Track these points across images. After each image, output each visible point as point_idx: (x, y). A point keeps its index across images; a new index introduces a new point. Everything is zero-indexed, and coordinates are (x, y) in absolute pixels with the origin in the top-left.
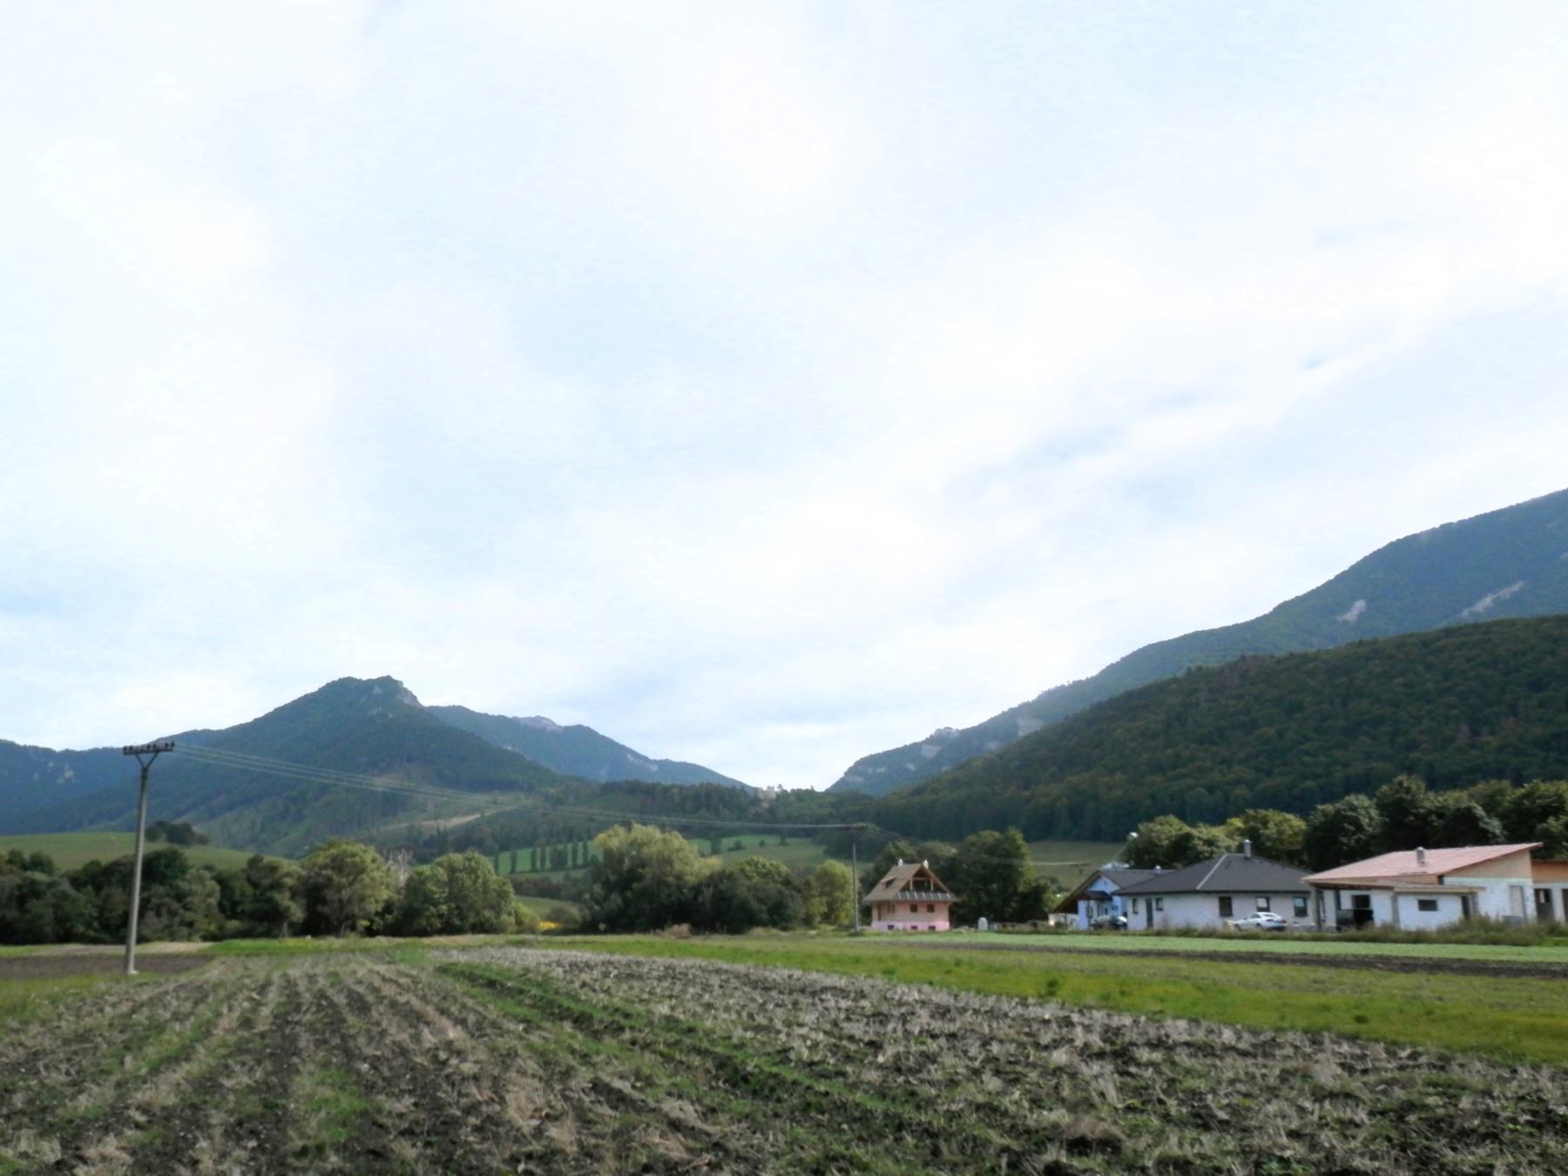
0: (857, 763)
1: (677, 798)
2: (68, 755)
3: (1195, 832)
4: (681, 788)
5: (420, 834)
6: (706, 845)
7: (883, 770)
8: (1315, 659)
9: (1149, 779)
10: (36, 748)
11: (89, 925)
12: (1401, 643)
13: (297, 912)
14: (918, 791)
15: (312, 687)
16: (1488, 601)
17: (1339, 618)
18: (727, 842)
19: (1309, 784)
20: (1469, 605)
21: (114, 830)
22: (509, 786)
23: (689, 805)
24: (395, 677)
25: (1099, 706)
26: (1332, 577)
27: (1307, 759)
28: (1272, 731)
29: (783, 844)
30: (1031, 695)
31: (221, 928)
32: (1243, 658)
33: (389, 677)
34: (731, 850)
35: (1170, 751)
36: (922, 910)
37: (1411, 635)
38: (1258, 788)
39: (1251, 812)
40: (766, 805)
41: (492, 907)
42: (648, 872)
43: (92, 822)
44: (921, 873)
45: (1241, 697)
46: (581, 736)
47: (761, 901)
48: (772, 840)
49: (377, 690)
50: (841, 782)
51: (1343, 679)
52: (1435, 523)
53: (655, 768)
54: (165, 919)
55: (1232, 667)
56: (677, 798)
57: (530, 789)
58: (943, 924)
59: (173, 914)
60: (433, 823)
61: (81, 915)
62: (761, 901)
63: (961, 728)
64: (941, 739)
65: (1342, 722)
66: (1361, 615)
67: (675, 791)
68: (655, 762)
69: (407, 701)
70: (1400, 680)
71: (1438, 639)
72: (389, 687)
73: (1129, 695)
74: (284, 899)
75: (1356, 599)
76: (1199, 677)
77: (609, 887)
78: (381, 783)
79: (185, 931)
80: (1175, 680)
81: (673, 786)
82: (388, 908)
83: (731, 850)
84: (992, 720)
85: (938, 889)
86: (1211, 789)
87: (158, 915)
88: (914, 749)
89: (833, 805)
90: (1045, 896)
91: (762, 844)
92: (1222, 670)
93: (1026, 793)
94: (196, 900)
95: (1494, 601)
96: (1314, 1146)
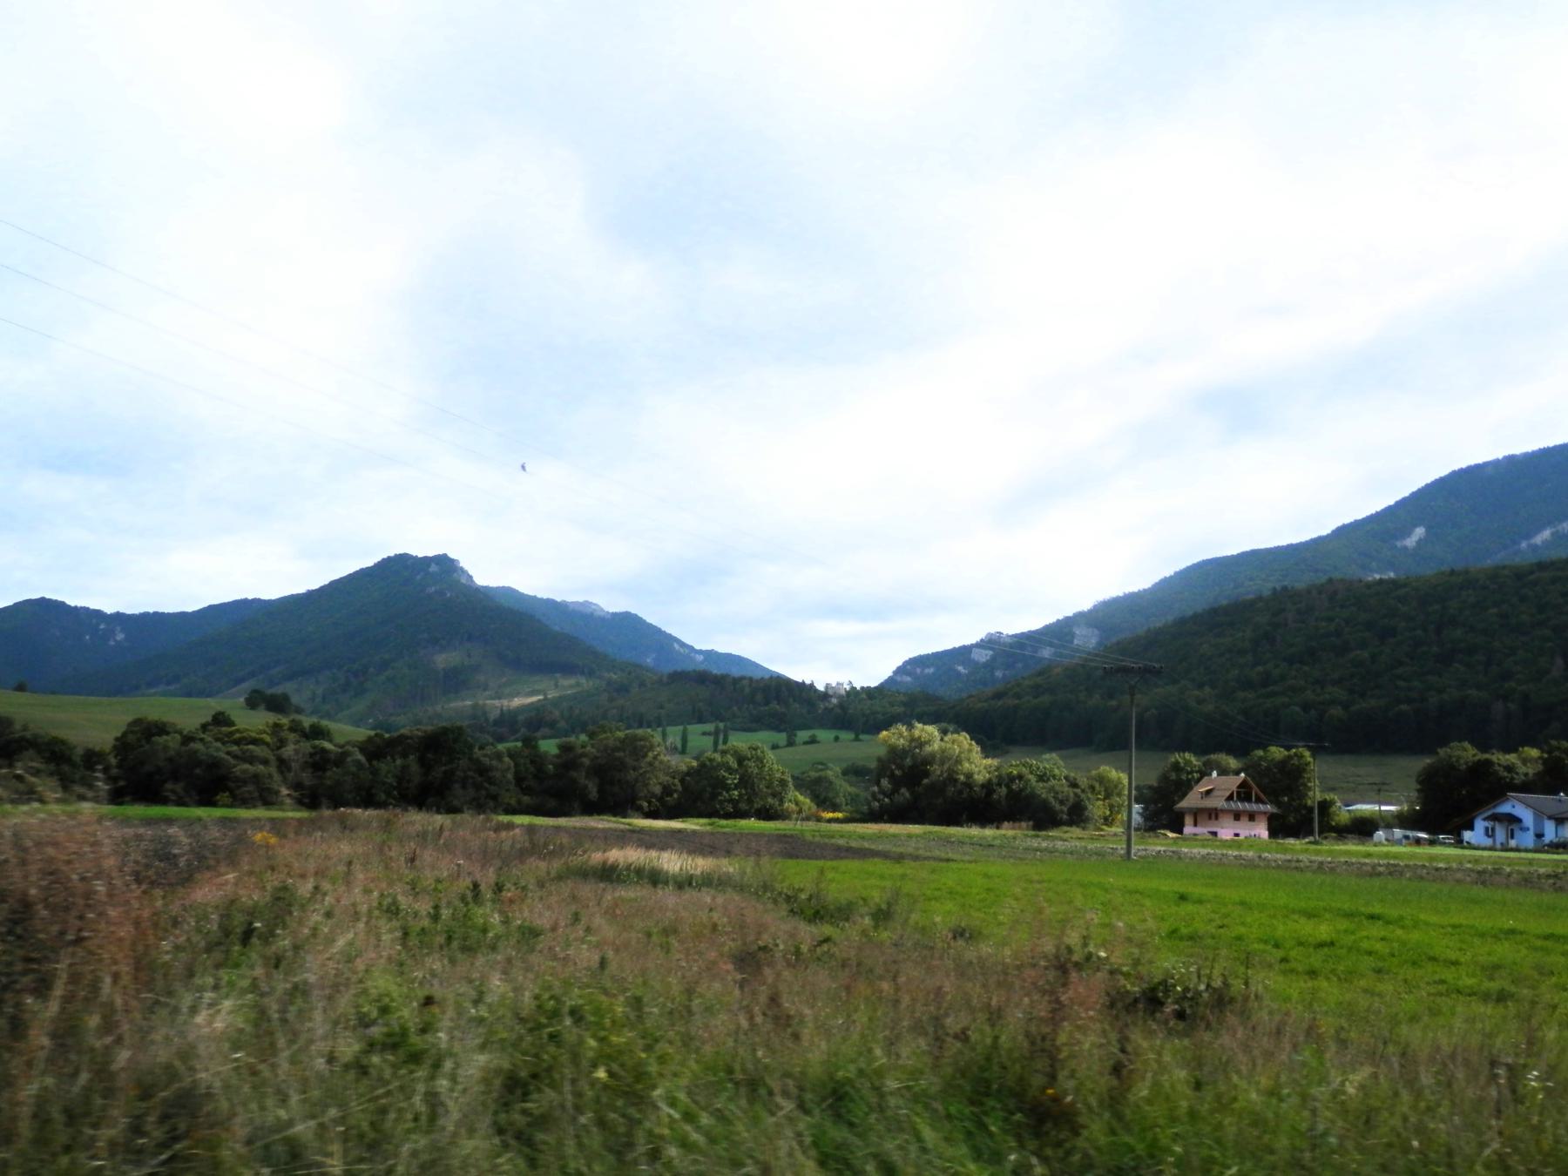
0: (906, 663)
1: (747, 690)
2: (119, 617)
3: (1494, 758)
4: (751, 679)
5: (485, 713)
6: (781, 738)
7: (931, 670)
8: (1405, 585)
9: (1241, 694)
10: (86, 609)
11: (388, 794)
12: (1495, 574)
13: (593, 792)
14: (999, 695)
15: (370, 562)
16: (1546, 534)
17: (1399, 544)
18: (803, 735)
19: (1404, 707)
20: (1528, 536)
21: (174, 694)
22: (568, 669)
23: (759, 697)
24: (452, 555)
25: (1182, 622)
26: (1392, 502)
27: (1401, 683)
28: (1366, 655)
29: (857, 739)
30: (1086, 605)
31: (519, 802)
32: (1330, 581)
33: (445, 556)
34: (805, 743)
35: (1260, 668)
36: (1245, 819)
37: (1504, 567)
38: (1354, 708)
39: (1554, 743)
40: (834, 701)
41: (774, 795)
42: (936, 770)
43: (150, 685)
44: (1243, 785)
45: (1330, 619)
46: (628, 622)
47: (1062, 802)
48: (846, 736)
49: (433, 568)
50: (890, 681)
51: (1437, 607)
52: (1498, 453)
53: (700, 658)
54: (471, 792)
55: (1320, 589)
56: (747, 690)
57: (591, 674)
58: (1264, 833)
59: (478, 787)
60: (497, 703)
61: (384, 783)
62: (1062, 802)
63: (612, 610)
64: (990, 642)
65: (1435, 649)
66: (1419, 542)
67: (745, 682)
68: (700, 652)
69: (463, 581)
70: (1495, 610)
71: (1532, 573)
72: (445, 565)
73: (1214, 611)
74: (581, 777)
75: (1416, 526)
76: (1283, 597)
77: (897, 783)
78: (443, 660)
79: (491, 804)
80: (1260, 598)
81: (742, 678)
82: (667, 790)
83: (805, 743)
84: (1047, 627)
85: (1259, 800)
86: (1306, 707)
87: (464, 787)
88: (962, 653)
89: (905, 704)
90: (1333, 809)
91: (837, 739)
92: (1309, 592)
93: (1114, 703)
94: (498, 774)
95: (1552, 534)
96: (1162, 1047)
